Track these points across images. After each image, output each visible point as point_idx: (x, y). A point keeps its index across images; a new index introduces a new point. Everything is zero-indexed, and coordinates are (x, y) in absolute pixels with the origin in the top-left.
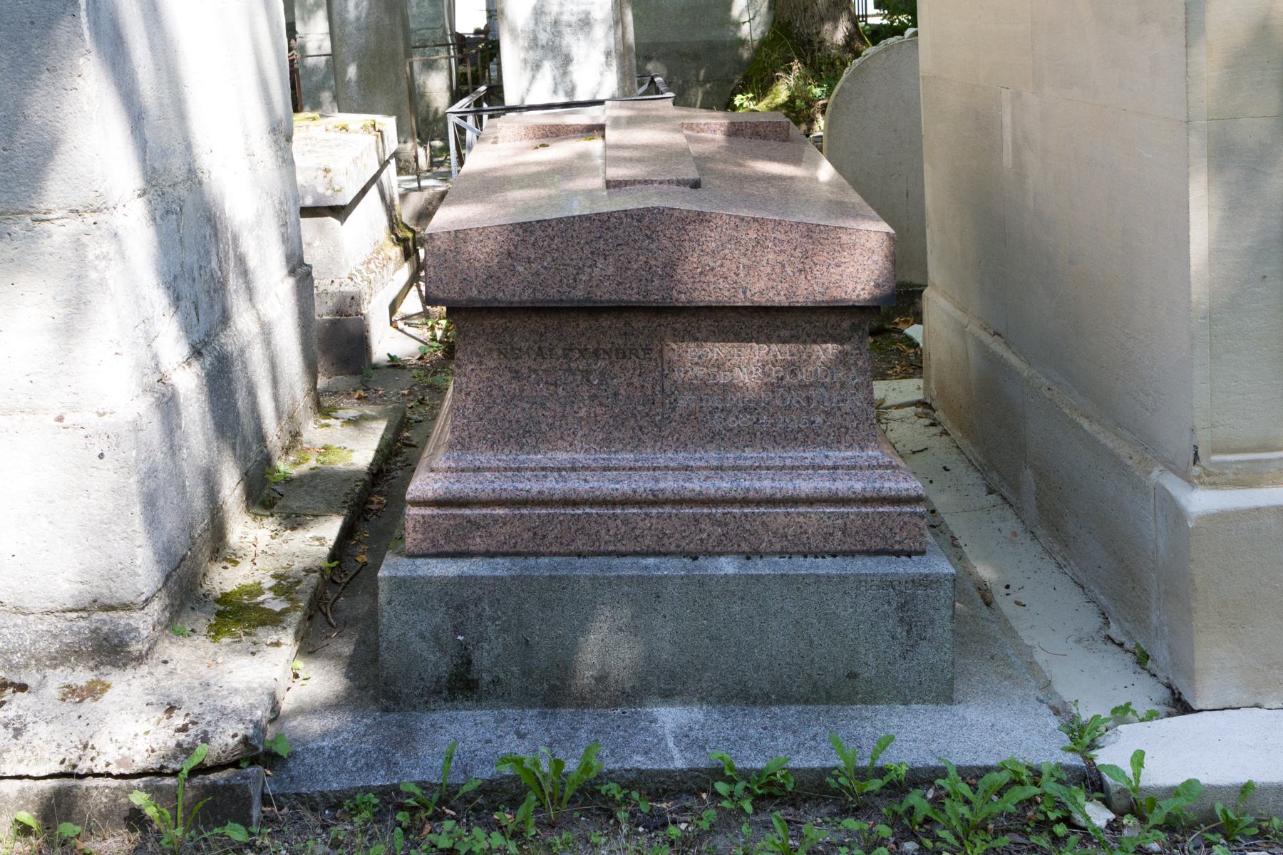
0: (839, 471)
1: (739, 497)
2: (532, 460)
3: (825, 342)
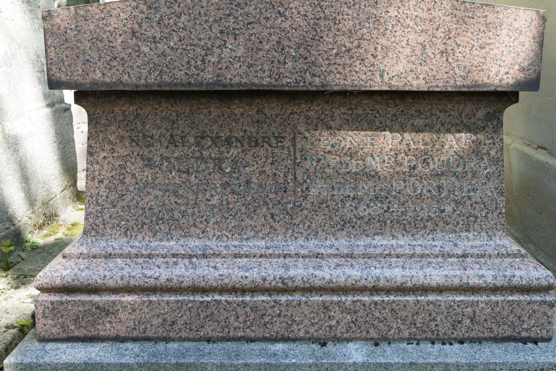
0: (469, 260)
1: (369, 285)
2: (164, 247)
3: (459, 131)
